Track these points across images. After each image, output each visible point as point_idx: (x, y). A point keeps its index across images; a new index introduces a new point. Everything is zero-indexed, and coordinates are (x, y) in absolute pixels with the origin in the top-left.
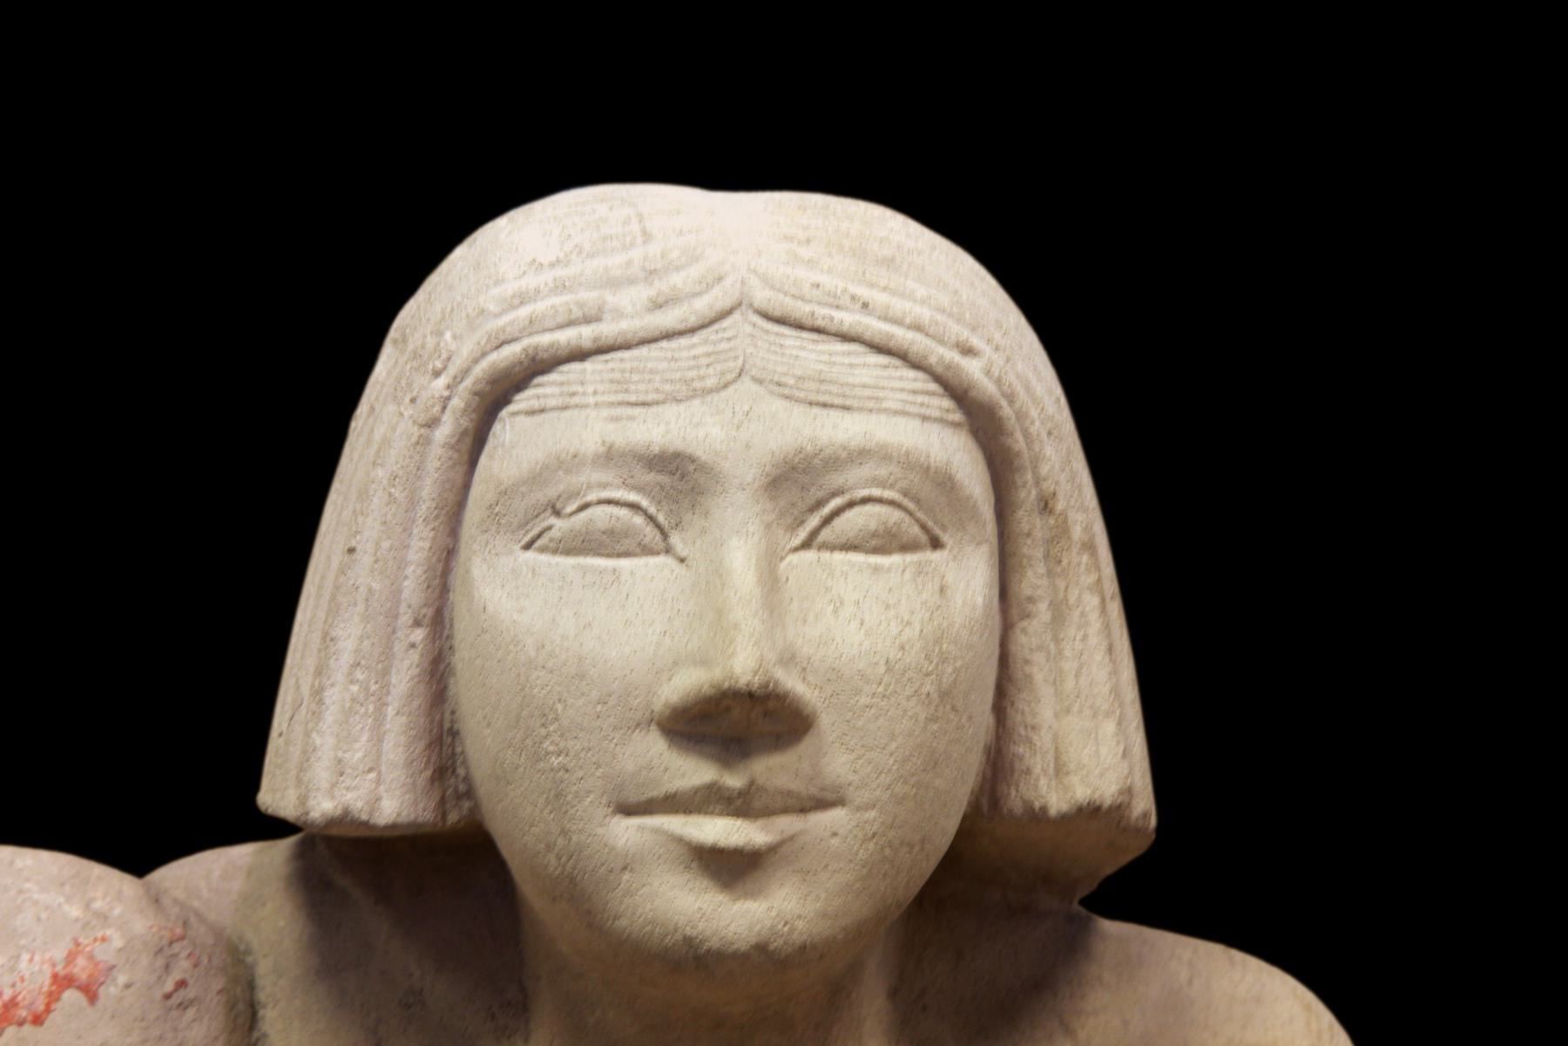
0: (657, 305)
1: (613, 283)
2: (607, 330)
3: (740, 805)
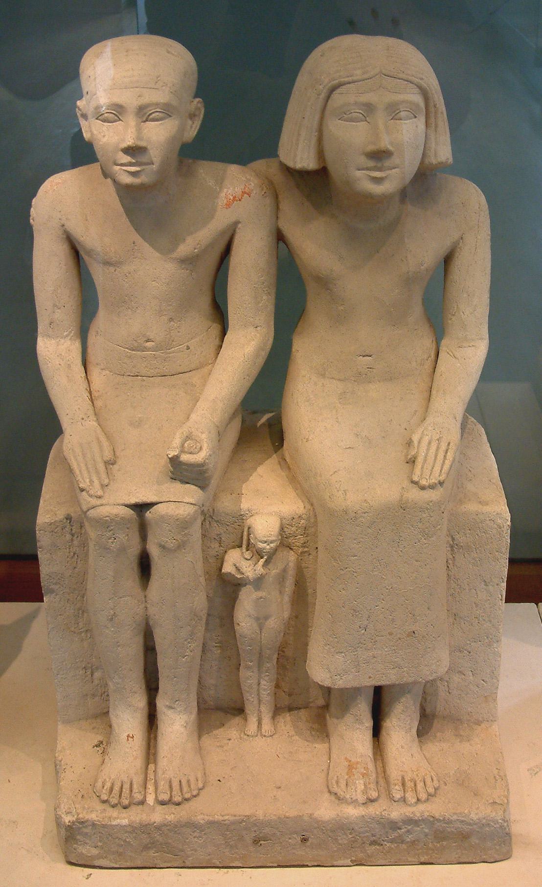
0: (364, 73)
2: (355, 78)
3: (380, 169)
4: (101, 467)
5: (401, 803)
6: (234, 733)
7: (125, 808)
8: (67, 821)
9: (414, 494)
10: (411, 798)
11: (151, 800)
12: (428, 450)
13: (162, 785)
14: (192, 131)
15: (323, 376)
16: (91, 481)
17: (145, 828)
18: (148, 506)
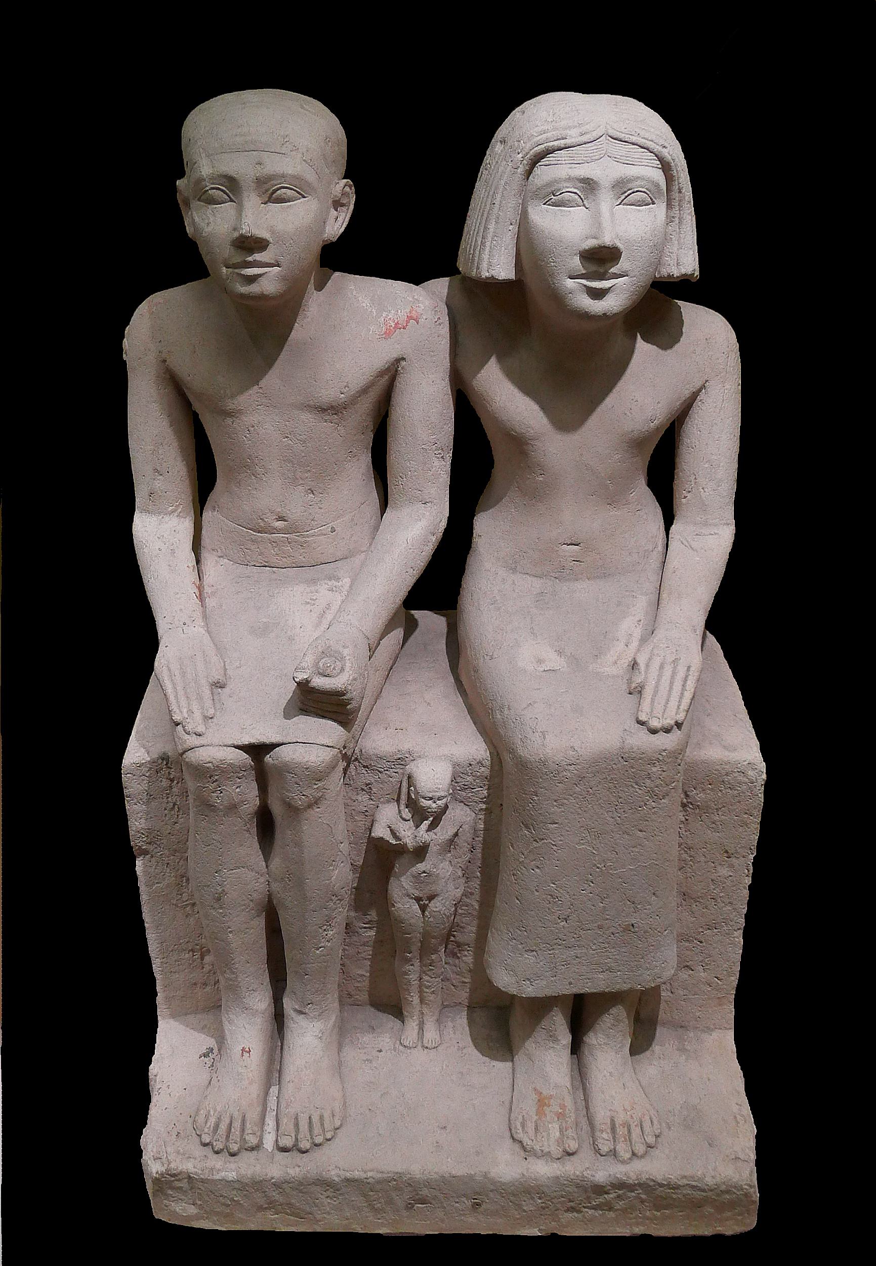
1: (569, 128)
2: (568, 142)
3: (602, 277)
4: (207, 692)
5: (611, 1159)
6: (385, 1041)
7: (233, 1155)
8: (154, 1171)
9: (641, 740)
10: (623, 1151)
11: (269, 1142)
12: (660, 676)
13: (287, 1124)
14: (336, 225)
15: (514, 570)
16: (191, 712)
17: (258, 1185)
18: (269, 748)
